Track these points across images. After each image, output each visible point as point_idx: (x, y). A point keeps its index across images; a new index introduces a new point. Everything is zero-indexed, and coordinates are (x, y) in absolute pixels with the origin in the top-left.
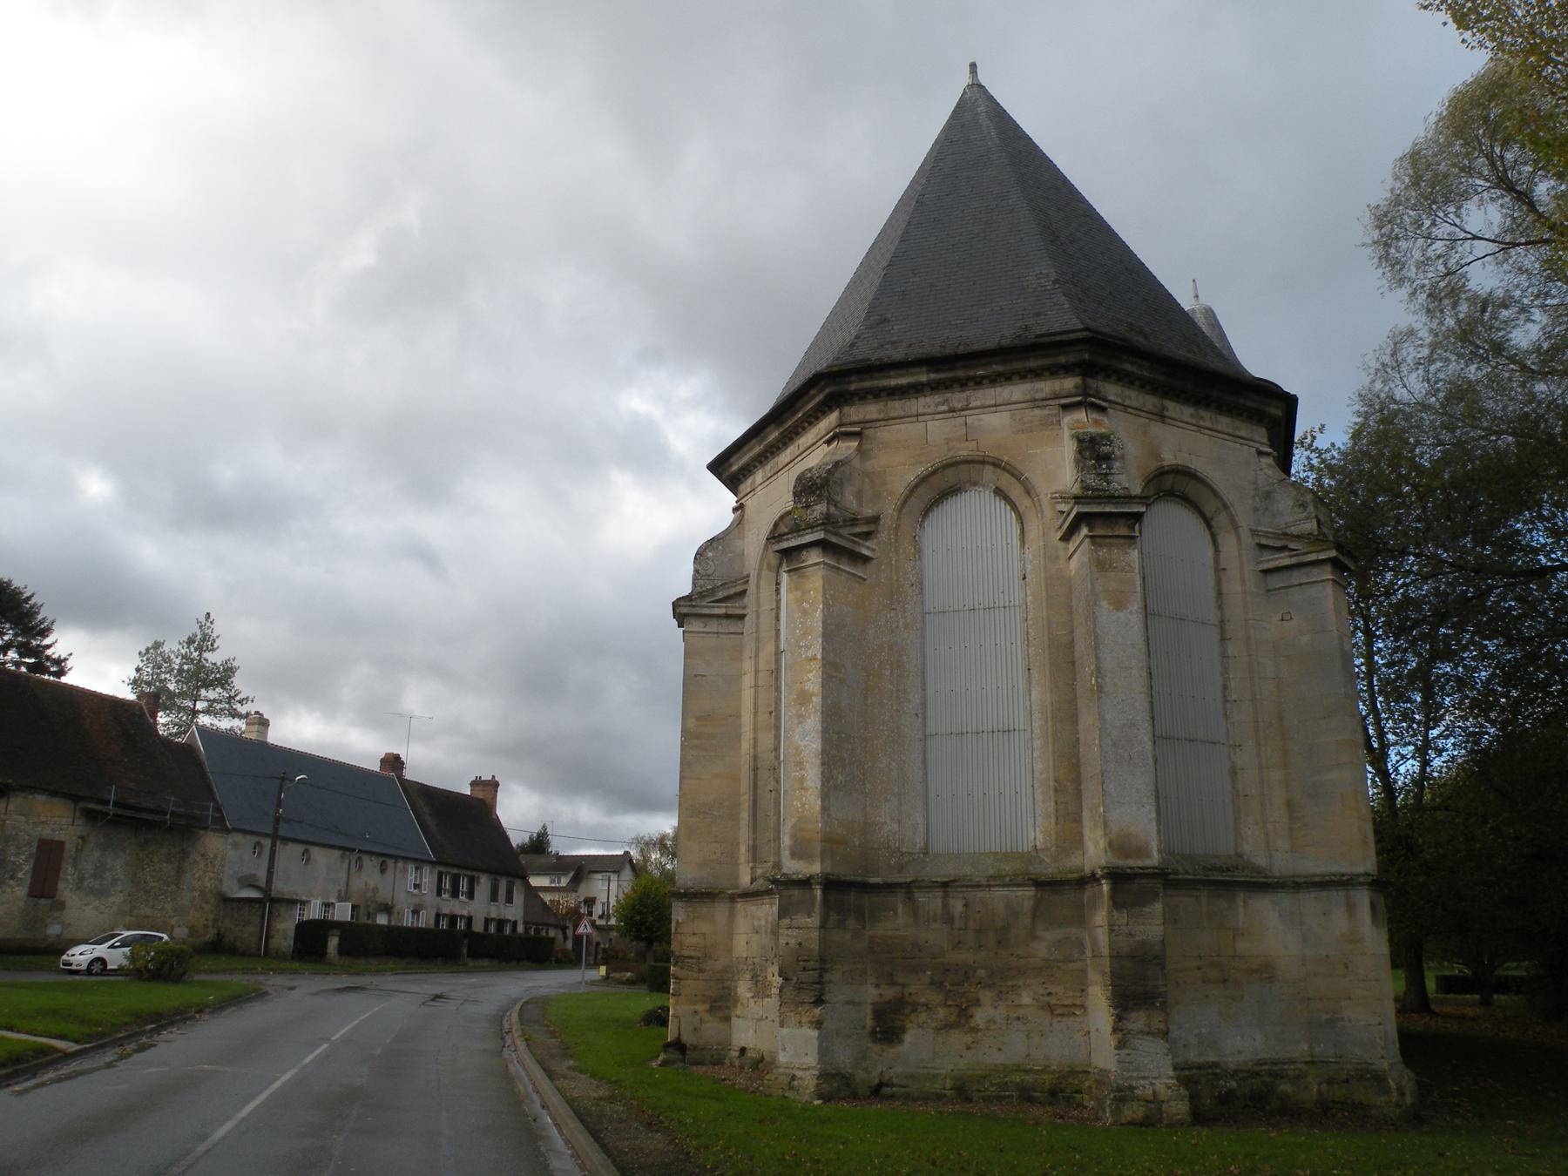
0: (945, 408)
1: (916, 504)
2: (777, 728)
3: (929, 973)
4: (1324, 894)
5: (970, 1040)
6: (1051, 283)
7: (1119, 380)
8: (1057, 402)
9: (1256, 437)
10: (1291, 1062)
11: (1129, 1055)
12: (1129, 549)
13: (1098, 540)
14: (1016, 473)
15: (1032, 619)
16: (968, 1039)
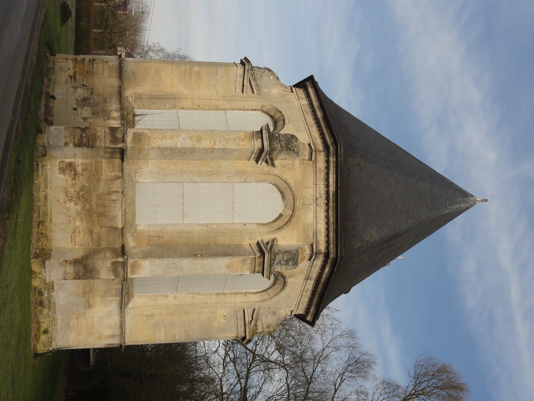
1: (279, 182)
2: (193, 109)
4: (118, 326)
5: (61, 201)
6: (368, 240)
7: (322, 265)
8: (315, 242)
10: (55, 313)
11: (57, 266)
12: (250, 271)
13: (254, 259)
14: (287, 224)
15: (227, 227)
16: (62, 201)
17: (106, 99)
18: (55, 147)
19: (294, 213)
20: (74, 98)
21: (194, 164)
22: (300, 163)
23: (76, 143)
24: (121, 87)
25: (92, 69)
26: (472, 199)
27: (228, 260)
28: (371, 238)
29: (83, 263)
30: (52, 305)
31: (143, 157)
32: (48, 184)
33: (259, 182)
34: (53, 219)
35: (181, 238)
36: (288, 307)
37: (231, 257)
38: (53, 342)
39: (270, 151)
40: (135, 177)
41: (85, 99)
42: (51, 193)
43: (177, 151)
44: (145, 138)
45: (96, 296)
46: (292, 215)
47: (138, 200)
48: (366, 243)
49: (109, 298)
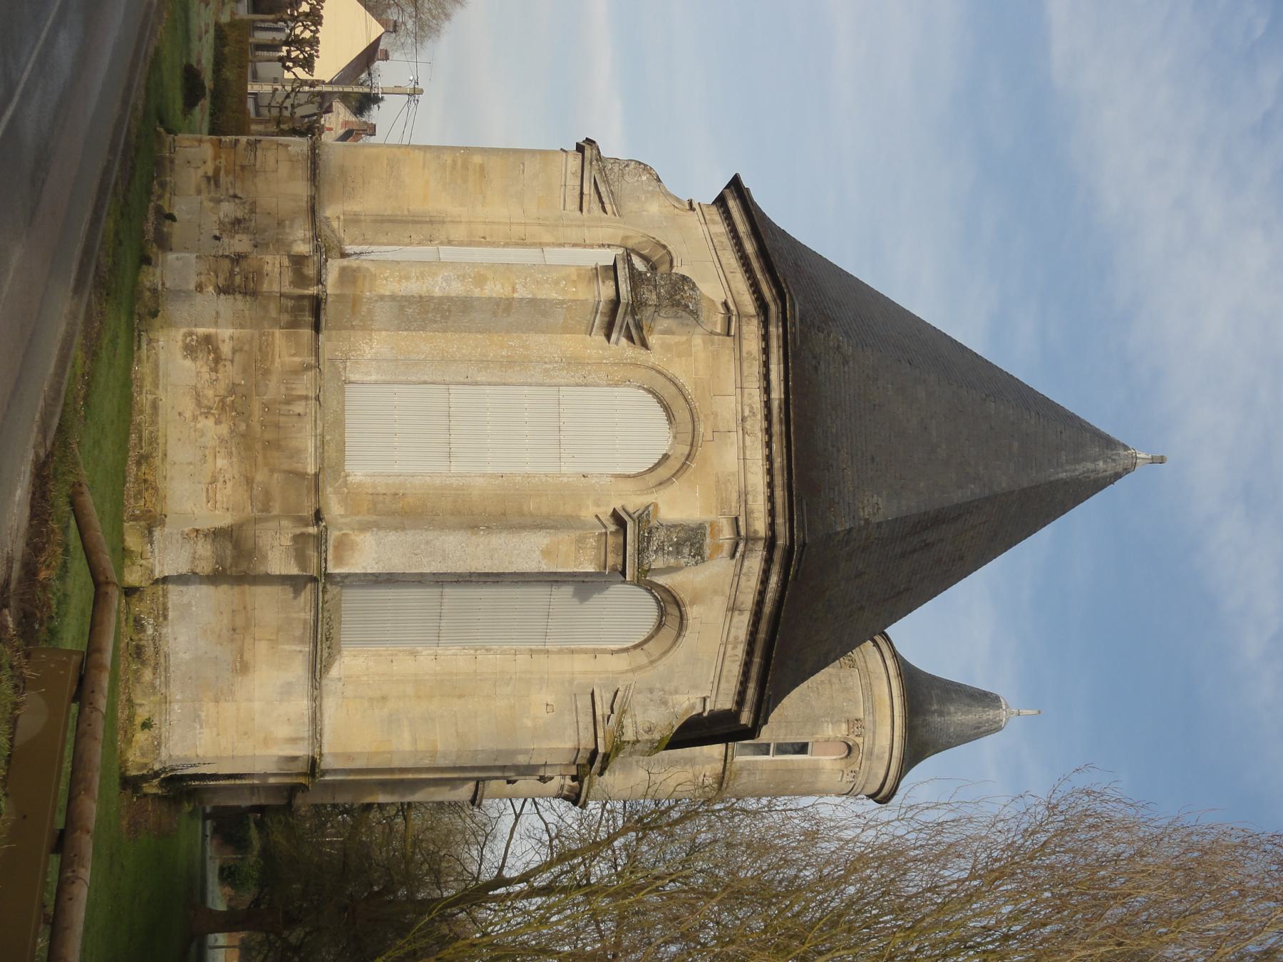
0: (747, 413)
1: (660, 383)
2: (470, 244)
3: (243, 382)
4: (306, 720)
5: (187, 416)
8: (743, 513)
9: (721, 697)
10: (167, 684)
11: (178, 542)
13: (604, 538)
15: (546, 481)
16: (188, 414)
17: (283, 221)
18: (180, 294)
19: (694, 448)
20: (215, 218)
21: (471, 342)
22: (704, 342)
23: (221, 286)
24: (314, 199)
25: (252, 162)
26: (1126, 453)
27: (545, 537)
28: (874, 514)
29: (232, 536)
30: (162, 660)
31: (361, 324)
32: (161, 377)
33: (616, 385)
34: (169, 452)
35: (443, 499)
36: (695, 687)
37: (552, 531)
38: (163, 748)
39: (632, 304)
40: (345, 368)
41: (237, 222)
42: (165, 400)
43: (432, 306)
44: (365, 277)
45: (258, 640)
46: (689, 455)
47: (350, 419)
48: (862, 523)
49: (287, 647)
